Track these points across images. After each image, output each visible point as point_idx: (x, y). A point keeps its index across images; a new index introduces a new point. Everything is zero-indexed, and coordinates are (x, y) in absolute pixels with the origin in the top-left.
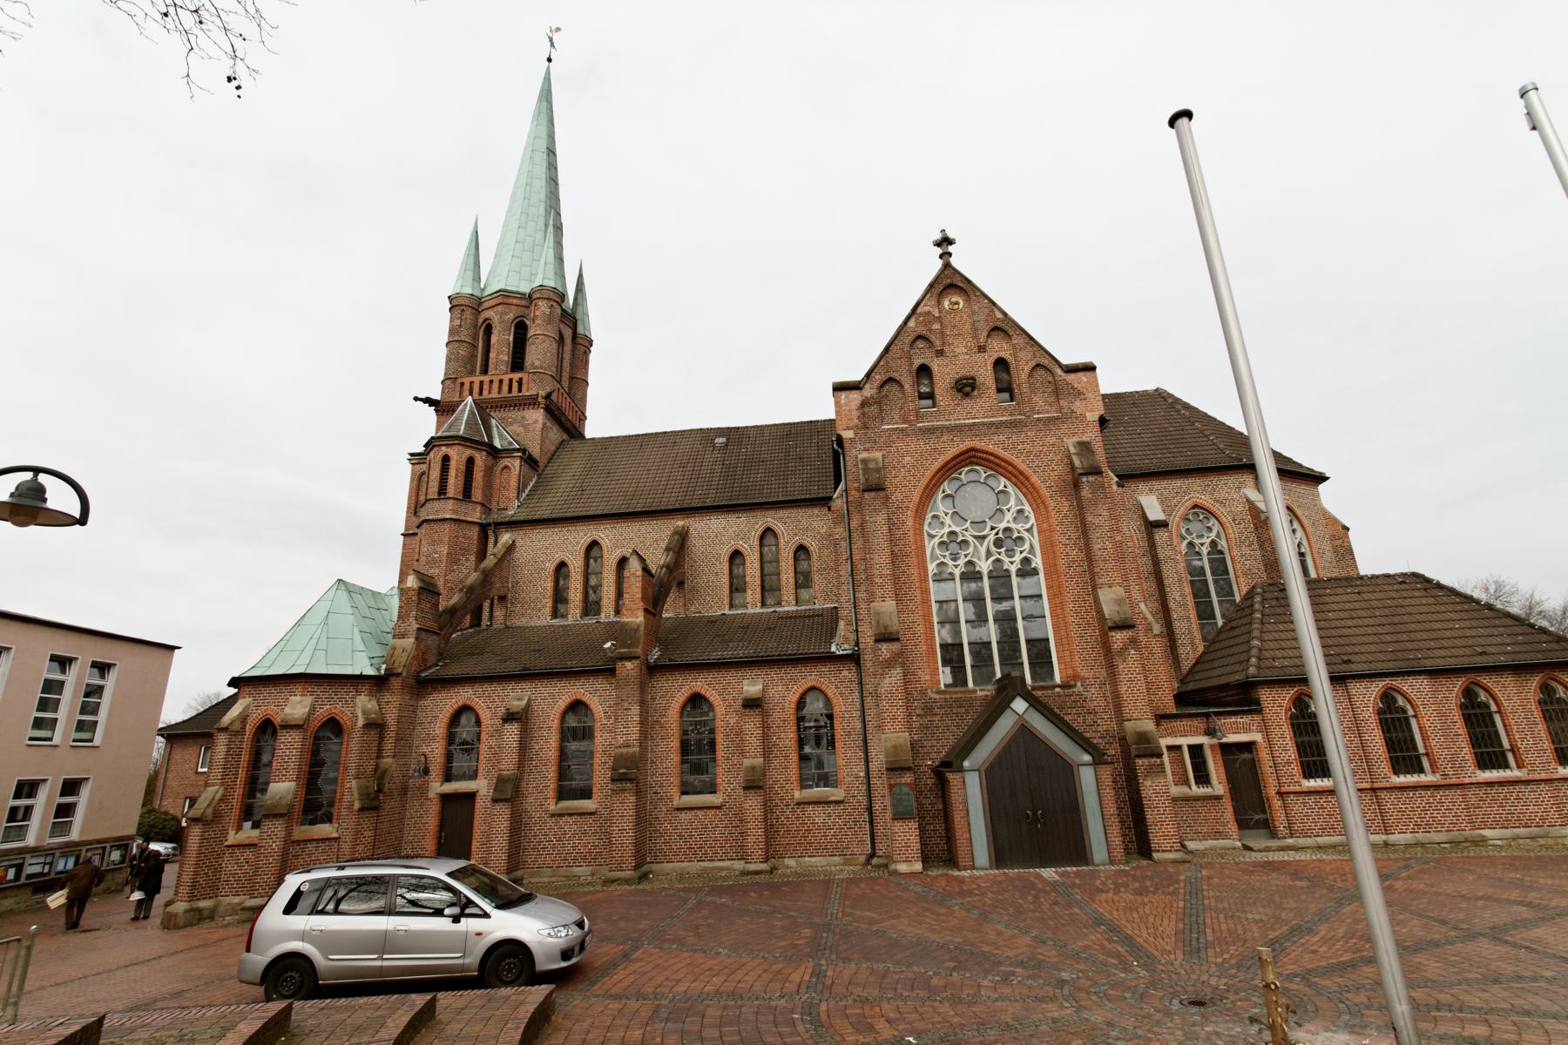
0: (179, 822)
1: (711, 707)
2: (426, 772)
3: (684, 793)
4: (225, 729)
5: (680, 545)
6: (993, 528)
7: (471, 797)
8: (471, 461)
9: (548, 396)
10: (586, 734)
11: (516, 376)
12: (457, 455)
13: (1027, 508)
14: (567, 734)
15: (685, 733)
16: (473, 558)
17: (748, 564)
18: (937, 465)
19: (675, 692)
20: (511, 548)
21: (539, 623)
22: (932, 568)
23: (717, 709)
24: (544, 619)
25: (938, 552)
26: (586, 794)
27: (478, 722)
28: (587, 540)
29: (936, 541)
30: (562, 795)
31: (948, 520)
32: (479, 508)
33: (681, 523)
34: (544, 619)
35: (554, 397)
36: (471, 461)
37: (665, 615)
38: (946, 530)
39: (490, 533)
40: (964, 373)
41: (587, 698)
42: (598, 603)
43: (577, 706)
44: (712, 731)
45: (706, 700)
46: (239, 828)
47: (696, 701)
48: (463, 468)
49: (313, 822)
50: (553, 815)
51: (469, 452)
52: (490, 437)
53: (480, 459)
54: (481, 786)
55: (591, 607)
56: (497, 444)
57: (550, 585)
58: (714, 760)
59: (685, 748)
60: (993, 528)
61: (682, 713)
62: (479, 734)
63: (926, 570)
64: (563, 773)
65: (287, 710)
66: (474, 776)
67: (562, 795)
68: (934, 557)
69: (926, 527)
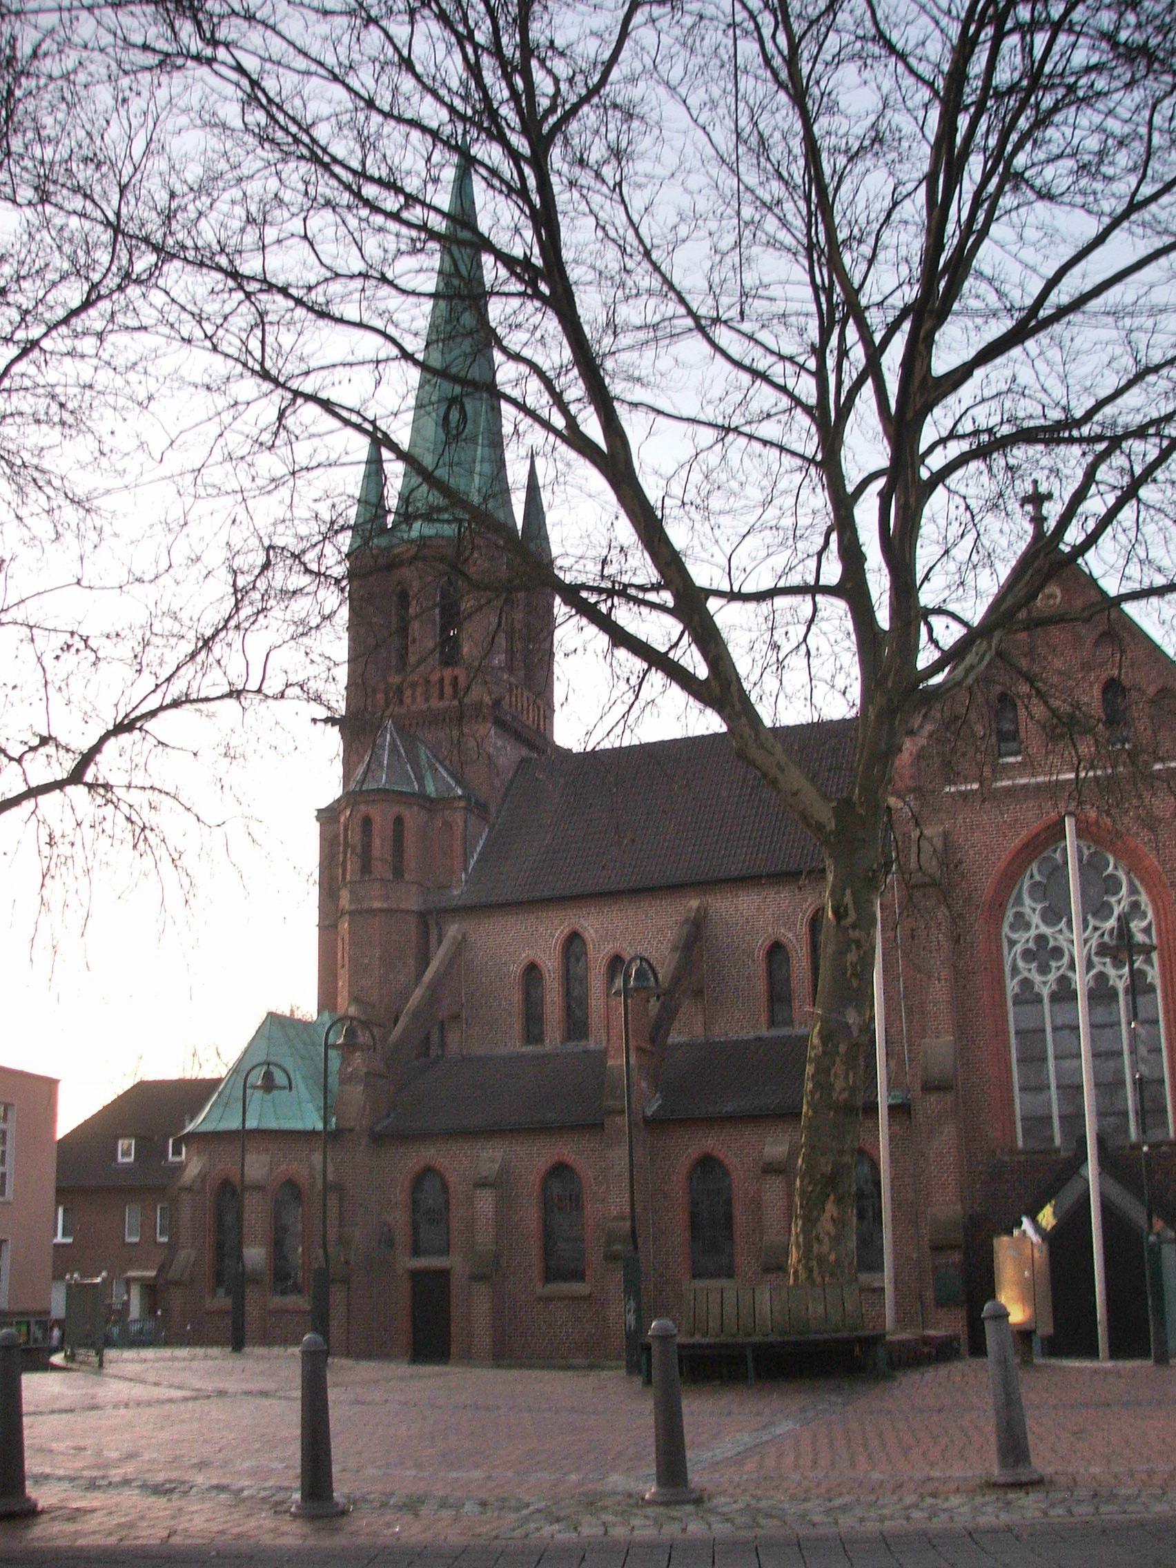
0: (47, 1330)
1: (726, 1173)
2: (391, 1244)
3: (694, 1277)
4: (189, 1189)
5: (695, 936)
6: (1096, 929)
7: (444, 1274)
8: (399, 821)
9: (497, 703)
10: (575, 1201)
11: (448, 673)
12: (381, 816)
13: (1144, 898)
14: (548, 1205)
15: (694, 1203)
16: (412, 962)
17: (794, 962)
18: (1015, 843)
19: (687, 1148)
20: (461, 945)
21: (503, 1051)
22: (1012, 986)
23: (734, 1175)
24: (514, 1045)
25: (1020, 964)
26: (578, 1275)
27: (445, 1187)
28: (560, 932)
29: (1018, 948)
30: (550, 1275)
31: (1036, 919)
32: (414, 888)
33: (694, 903)
34: (514, 1045)
35: (505, 704)
36: (399, 821)
37: (670, 1041)
38: (1033, 932)
39: (432, 922)
40: (768, 943)
41: (721, 1152)
42: (585, 1024)
43: (560, 1170)
44: (729, 1202)
45: (720, 1163)
46: (214, 1295)
47: (707, 1164)
48: (390, 833)
49: (284, 1293)
50: (540, 1299)
51: (396, 809)
52: (422, 785)
53: (413, 818)
54: (453, 1262)
55: (576, 1026)
56: (431, 789)
57: (516, 997)
58: (730, 1237)
59: (695, 1224)
60: (1096, 929)
61: (690, 1178)
62: (447, 1202)
63: (1002, 988)
64: (548, 1250)
65: (499, 1154)
66: (445, 1251)
67: (550, 1275)
68: (1015, 970)
69: (1006, 929)
